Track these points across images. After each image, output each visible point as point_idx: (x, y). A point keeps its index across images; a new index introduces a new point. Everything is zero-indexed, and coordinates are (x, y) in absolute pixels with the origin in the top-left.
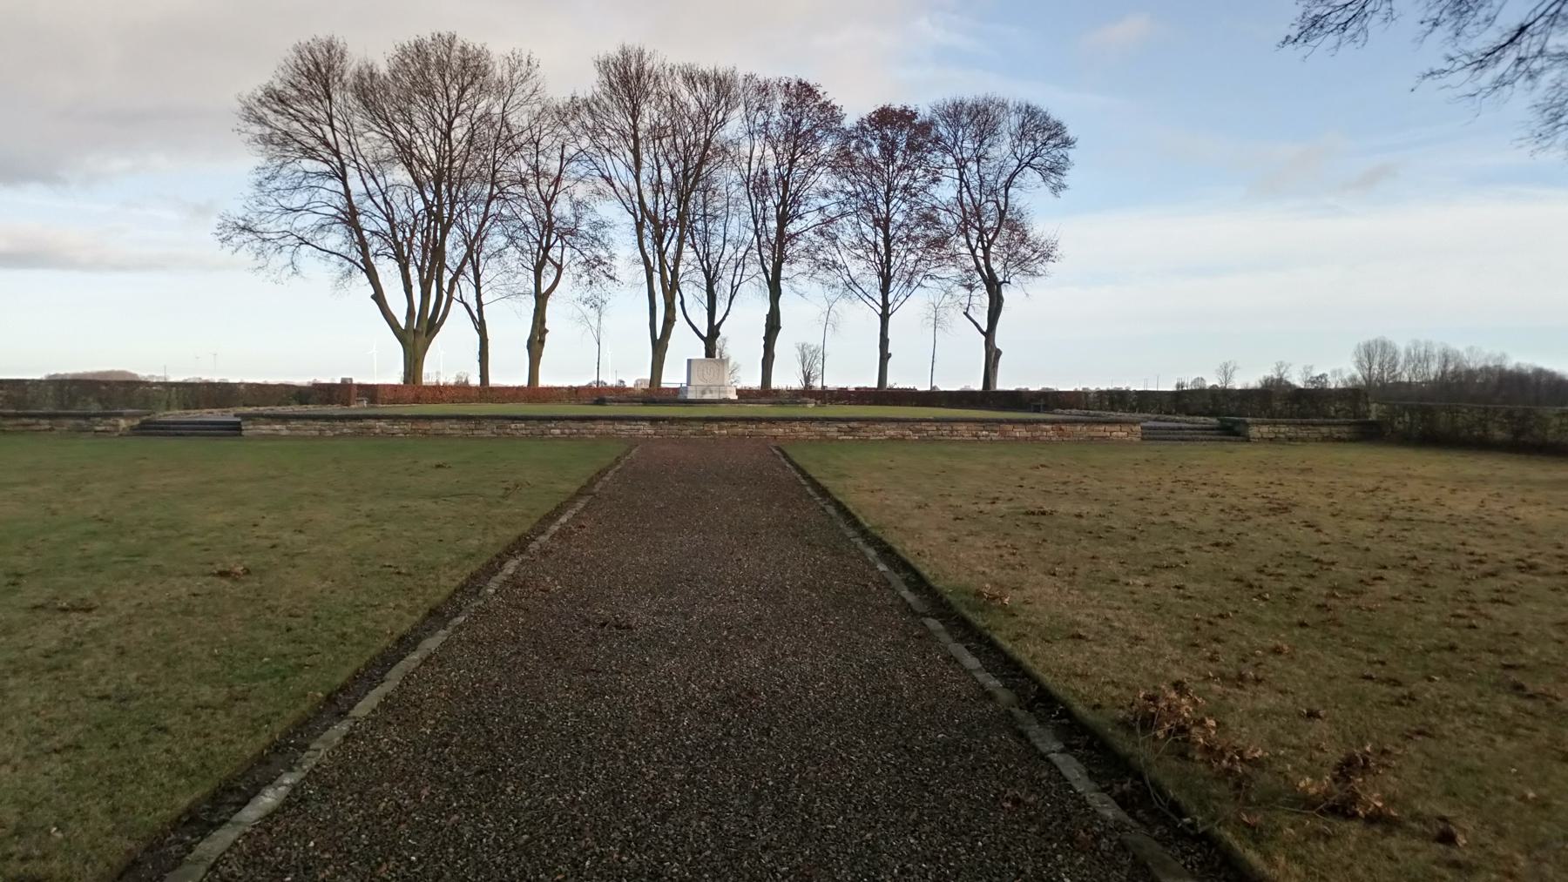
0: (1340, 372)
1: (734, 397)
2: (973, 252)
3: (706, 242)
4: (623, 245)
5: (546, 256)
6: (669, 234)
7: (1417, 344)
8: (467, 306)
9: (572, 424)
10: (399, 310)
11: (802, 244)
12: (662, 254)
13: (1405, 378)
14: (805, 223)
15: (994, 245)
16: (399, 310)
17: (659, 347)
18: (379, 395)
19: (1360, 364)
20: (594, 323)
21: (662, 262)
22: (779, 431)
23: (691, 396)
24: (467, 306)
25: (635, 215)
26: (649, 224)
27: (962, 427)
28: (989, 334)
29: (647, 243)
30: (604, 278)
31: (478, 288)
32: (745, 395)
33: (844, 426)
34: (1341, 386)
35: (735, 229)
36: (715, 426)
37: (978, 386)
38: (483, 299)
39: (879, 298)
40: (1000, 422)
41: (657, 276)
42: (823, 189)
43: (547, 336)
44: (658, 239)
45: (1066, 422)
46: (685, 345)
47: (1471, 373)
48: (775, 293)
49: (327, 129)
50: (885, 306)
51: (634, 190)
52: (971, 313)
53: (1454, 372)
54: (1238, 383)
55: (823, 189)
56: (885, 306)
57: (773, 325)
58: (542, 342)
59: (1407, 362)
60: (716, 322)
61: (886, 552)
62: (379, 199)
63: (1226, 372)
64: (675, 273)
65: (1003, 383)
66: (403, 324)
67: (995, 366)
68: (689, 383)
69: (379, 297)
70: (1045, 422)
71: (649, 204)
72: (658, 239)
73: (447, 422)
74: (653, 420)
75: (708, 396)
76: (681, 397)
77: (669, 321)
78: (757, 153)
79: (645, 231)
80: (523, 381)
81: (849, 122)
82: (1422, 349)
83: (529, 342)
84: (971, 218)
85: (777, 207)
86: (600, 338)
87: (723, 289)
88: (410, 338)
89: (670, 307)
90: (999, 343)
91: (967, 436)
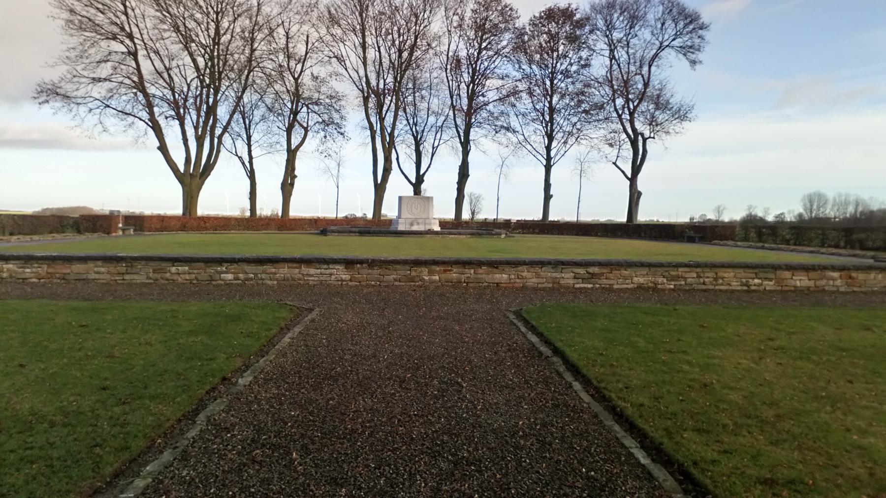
0: (793, 211)
1: (437, 228)
2: (620, 116)
3: (415, 115)
4: (354, 118)
5: (295, 119)
6: (387, 102)
7: (840, 195)
8: (240, 158)
9: (246, 267)
10: (180, 160)
11: (484, 114)
12: (382, 120)
13: (832, 215)
14: (492, 89)
15: (637, 109)
16: (180, 160)
17: (380, 189)
18: (146, 224)
20: (335, 172)
21: (383, 128)
22: (502, 277)
23: (401, 228)
24: (240, 158)
26: (372, 96)
27: (728, 274)
28: (633, 180)
29: (372, 112)
30: (336, 134)
31: (249, 146)
32: (443, 224)
33: (581, 271)
34: (793, 220)
35: (436, 102)
36: (425, 271)
37: (623, 218)
38: (254, 154)
39: (544, 152)
40: (775, 268)
42: (505, 72)
43: (296, 180)
44: (380, 106)
45: (858, 268)
46: (398, 187)
47: (872, 212)
48: (466, 145)
49: (123, 18)
50: (549, 159)
51: (362, 72)
52: (618, 163)
53: (861, 213)
54: (726, 218)
55: (505, 72)
56: (549, 159)
58: (292, 185)
59: (833, 205)
60: (422, 173)
61: (600, 396)
62: (166, 75)
63: (719, 210)
64: (391, 135)
65: (643, 217)
66: (182, 168)
67: (637, 204)
68: (399, 217)
69: (163, 148)
70: (833, 268)
71: (373, 83)
72: (380, 106)
73: (91, 265)
74: (349, 263)
75: (415, 228)
76: (392, 228)
77: (387, 170)
78: (453, 47)
79: (371, 105)
80: (623, 218)
81: (523, 20)
82: (843, 198)
84: (622, 87)
85: (468, 87)
86: (335, 181)
87: (426, 148)
88: (187, 180)
89: (388, 160)
90: (640, 187)
91: (736, 285)
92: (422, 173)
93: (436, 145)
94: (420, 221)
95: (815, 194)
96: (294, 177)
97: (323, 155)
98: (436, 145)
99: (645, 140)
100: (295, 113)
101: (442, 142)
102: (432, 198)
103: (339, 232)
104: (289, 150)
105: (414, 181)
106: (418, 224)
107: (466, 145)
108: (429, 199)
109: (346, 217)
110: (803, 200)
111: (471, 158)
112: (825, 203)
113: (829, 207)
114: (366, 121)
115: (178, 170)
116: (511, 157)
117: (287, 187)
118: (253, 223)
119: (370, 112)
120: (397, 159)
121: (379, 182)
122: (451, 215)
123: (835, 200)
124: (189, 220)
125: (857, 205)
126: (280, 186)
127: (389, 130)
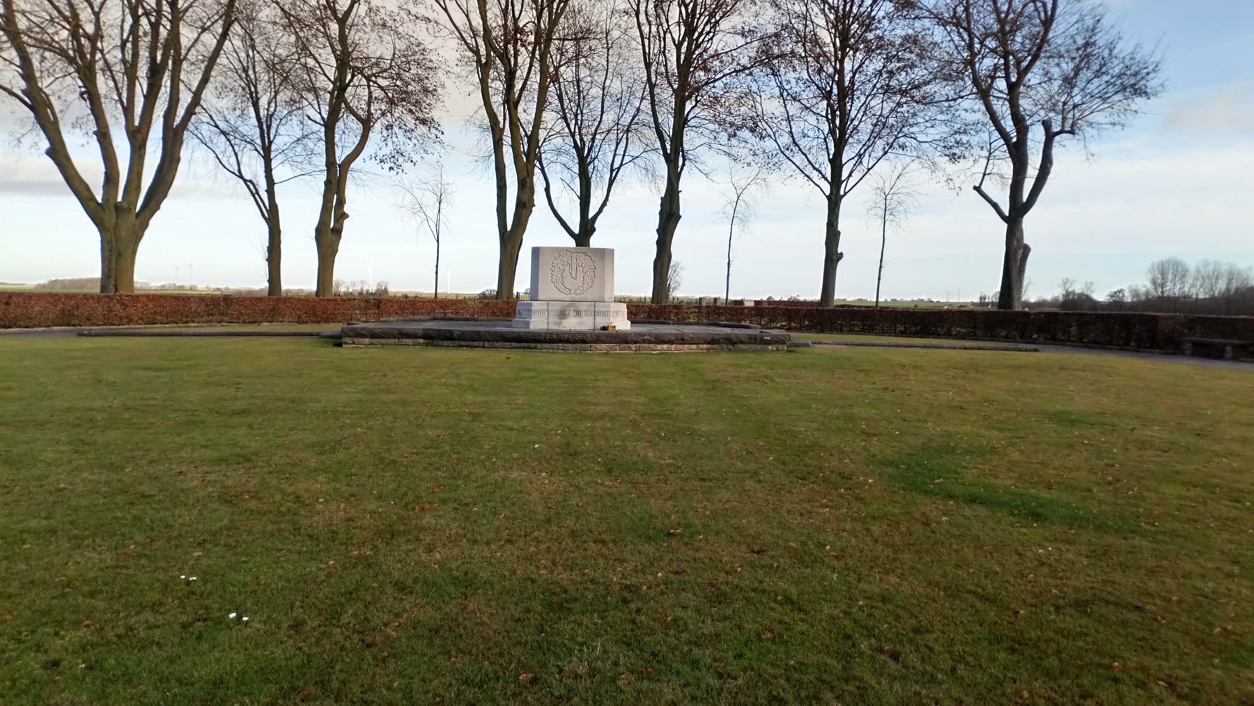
1: (622, 324)
4: (459, 100)
7: (1206, 263)
19: (1154, 282)
20: (432, 214)
21: (515, 124)
25: (476, 52)
26: (493, 54)
32: (636, 310)
38: (276, 175)
41: (507, 139)
43: (346, 223)
50: (836, 182)
52: (983, 188)
53: (1237, 289)
57: (669, 215)
58: (337, 232)
60: (590, 216)
64: (533, 138)
69: (58, 153)
75: (572, 324)
77: (525, 206)
82: (1211, 268)
83: (318, 230)
85: (678, 47)
86: (422, 227)
88: (110, 218)
89: (525, 185)
92: (590, 216)
93: (616, 165)
94: (583, 306)
95: (1168, 262)
96: (342, 216)
97: (386, 166)
98: (616, 165)
99: (1050, 137)
100: (340, 87)
101: (627, 159)
102: (612, 251)
103: (373, 335)
104: (330, 163)
105: (577, 231)
106: (578, 313)
107: (675, 156)
108: (605, 255)
109: (483, 294)
110: (1151, 271)
111: (686, 184)
112: (1184, 276)
113: (1189, 280)
114: (484, 112)
115: (93, 198)
116: (753, 187)
117: (328, 237)
118: (268, 308)
119: (493, 99)
120: (547, 190)
121: (509, 228)
122: (644, 290)
123: (1198, 271)
124: (111, 305)
125: (1230, 280)
126: (313, 234)
127: (530, 129)
